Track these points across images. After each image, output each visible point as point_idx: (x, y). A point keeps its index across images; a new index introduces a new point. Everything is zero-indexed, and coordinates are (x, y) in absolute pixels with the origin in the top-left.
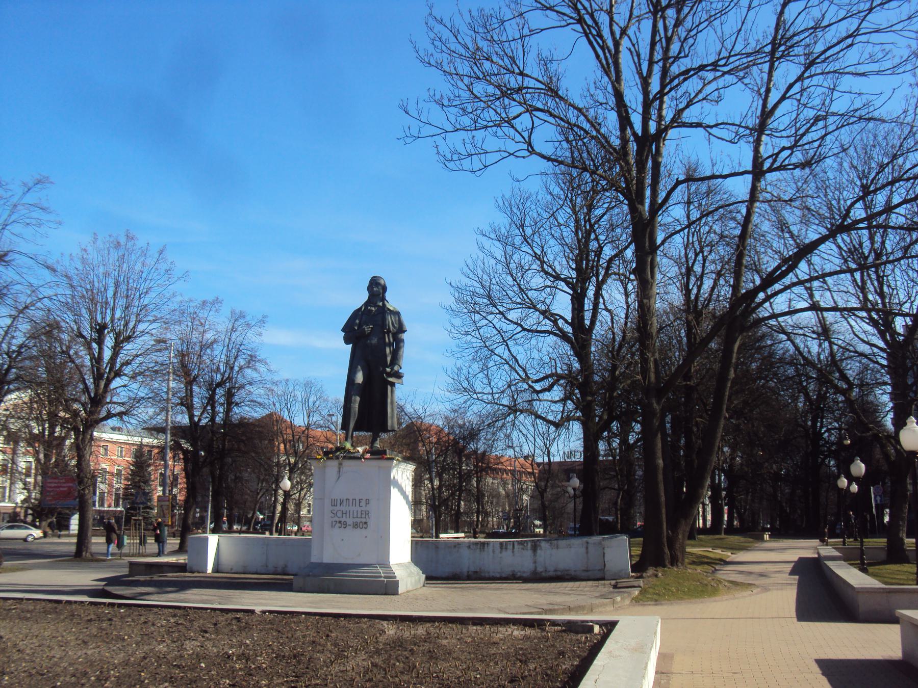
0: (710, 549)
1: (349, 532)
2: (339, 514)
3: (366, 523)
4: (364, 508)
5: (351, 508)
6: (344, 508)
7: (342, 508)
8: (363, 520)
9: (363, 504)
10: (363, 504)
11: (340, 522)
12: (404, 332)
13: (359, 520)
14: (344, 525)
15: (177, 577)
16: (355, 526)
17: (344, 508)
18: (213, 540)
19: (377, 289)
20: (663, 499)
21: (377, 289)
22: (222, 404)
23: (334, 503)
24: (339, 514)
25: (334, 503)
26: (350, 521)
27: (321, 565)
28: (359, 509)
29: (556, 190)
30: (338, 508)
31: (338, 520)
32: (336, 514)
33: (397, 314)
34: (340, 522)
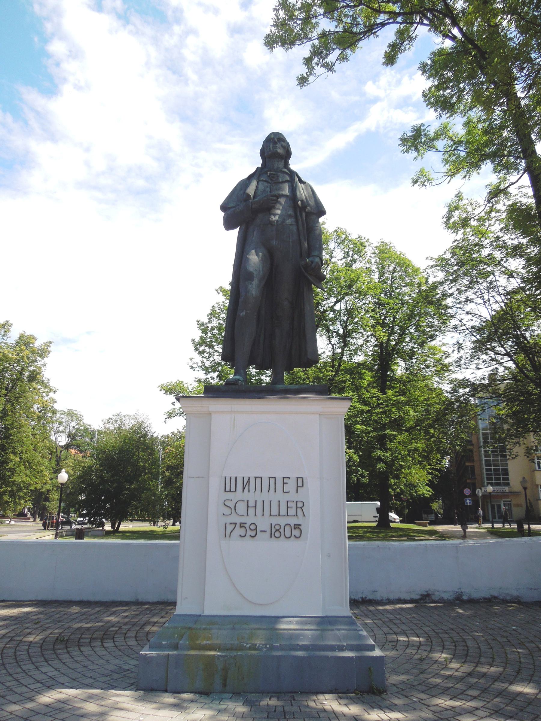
0: (146, 526)
1: (264, 546)
2: (241, 508)
3: (297, 526)
4: (292, 496)
5: (266, 496)
6: (251, 496)
7: (246, 496)
8: (293, 521)
9: (291, 486)
10: (291, 486)
11: (242, 525)
12: (322, 212)
13: (283, 521)
14: (251, 531)
16: (276, 532)
17: (251, 496)
19: (276, 151)
21: (276, 151)
23: (229, 485)
24: (241, 508)
25: (229, 485)
26: (263, 523)
27: (332, 693)
28: (284, 498)
29: (261, 273)
31: (238, 520)
34: (242, 525)
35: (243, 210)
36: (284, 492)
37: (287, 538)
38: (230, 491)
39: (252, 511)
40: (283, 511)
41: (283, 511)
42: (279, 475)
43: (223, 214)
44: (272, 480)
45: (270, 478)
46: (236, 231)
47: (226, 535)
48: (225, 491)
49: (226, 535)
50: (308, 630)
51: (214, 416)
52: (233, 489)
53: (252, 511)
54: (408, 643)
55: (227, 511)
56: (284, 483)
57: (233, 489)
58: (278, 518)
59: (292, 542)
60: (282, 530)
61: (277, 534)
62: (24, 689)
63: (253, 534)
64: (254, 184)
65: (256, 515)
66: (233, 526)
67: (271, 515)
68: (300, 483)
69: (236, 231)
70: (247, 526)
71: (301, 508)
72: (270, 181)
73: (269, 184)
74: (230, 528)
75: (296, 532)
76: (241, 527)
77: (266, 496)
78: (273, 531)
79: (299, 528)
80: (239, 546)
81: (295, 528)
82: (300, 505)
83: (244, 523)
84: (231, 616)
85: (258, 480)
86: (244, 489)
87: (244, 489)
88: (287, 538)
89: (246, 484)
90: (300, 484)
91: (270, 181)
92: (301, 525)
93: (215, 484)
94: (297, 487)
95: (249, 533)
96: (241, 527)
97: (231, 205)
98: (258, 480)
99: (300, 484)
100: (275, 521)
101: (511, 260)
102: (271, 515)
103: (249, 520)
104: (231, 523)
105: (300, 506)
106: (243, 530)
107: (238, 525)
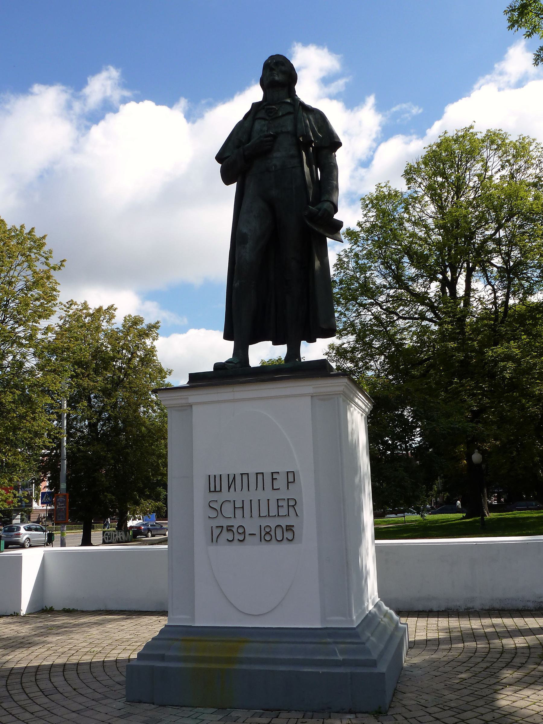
1: (254, 552)
2: (228, 510)
3: (289, 528)
4: (284, 494)
5: (255, 495)
6: (236, 495)
7: (231, 496)
8: (284, 522)
9: (281, 482)
10: (281, 482)
11: (229, 529)
14: (238, 535)
15: (59, 620)
16: (266, 536)
17: (236, 495)
18: (31, 560)
20: (306, 670)
22: (413, 279)
23: (214, 485)
24: (228, 510)
25: (214, 485)
28: (274, 496)
30: (225, 495)
31: (226, 523)
32: (220, 511)
33: (494, 139)
34: (229, 529)
35: (238, 159)
36: (273, 489)
37: (282, 540)
38: (215, 491)
39: (239, 512)
40: (273, 512)
41: (273, 512)
42: (267, 470)
43: (220, 165)
44: (260, 477)
45: (257, 474)
46: (234, 186)
47: (214, 539)
48: (210, 491)
49: (214, 539)
50: (311, 643)
51: (194, 407)
52: (218, 489)
53: (239, 512)
54: (487, 650)
55: (213, 514)
56: (273, 479)
57: (218, 489)
58: (267, 519)
59: (285, 547)
60: (273, 533)
61: (268, 538)
62: (37, 708)
63: (241, 538)
64: (258, 125)
65: (243, 516)
66: (220, 530)
67: (260, 516)
68: (291, 478)
69: (234, 186)
70: (235, 530)
71: (293, 506)
72: (267, 118)
73: (267, 122)
74: (216, 532)
75: (289, 535)
76: (228, 530)
77: (255, 495)
78: (263, 534)
79: (291, 530)
80: (229, 553)
81: (287, 530)
82: (292, 503)
83: (290, 526)
84: (264, 628)
85: (245, 477)
86: (229, 488)
87: (229, 488)
88: (292, 540)
89: (232, 482)
90: (291, 479)
91: (267, 118)
92: (293, 526)
93: (200, 486)
94: (288, 482)
95: (237, 537)
96: (228, 530)
97: (227, 154)
98: (245, 477)
99: (291, 479)
100: (265, 522)
101: (87, 90)
102: (260, 516)
103: (236, 523)
104: (217, 527)
105: (293, 505)
106: (231, 534)
107: (225, 529)
